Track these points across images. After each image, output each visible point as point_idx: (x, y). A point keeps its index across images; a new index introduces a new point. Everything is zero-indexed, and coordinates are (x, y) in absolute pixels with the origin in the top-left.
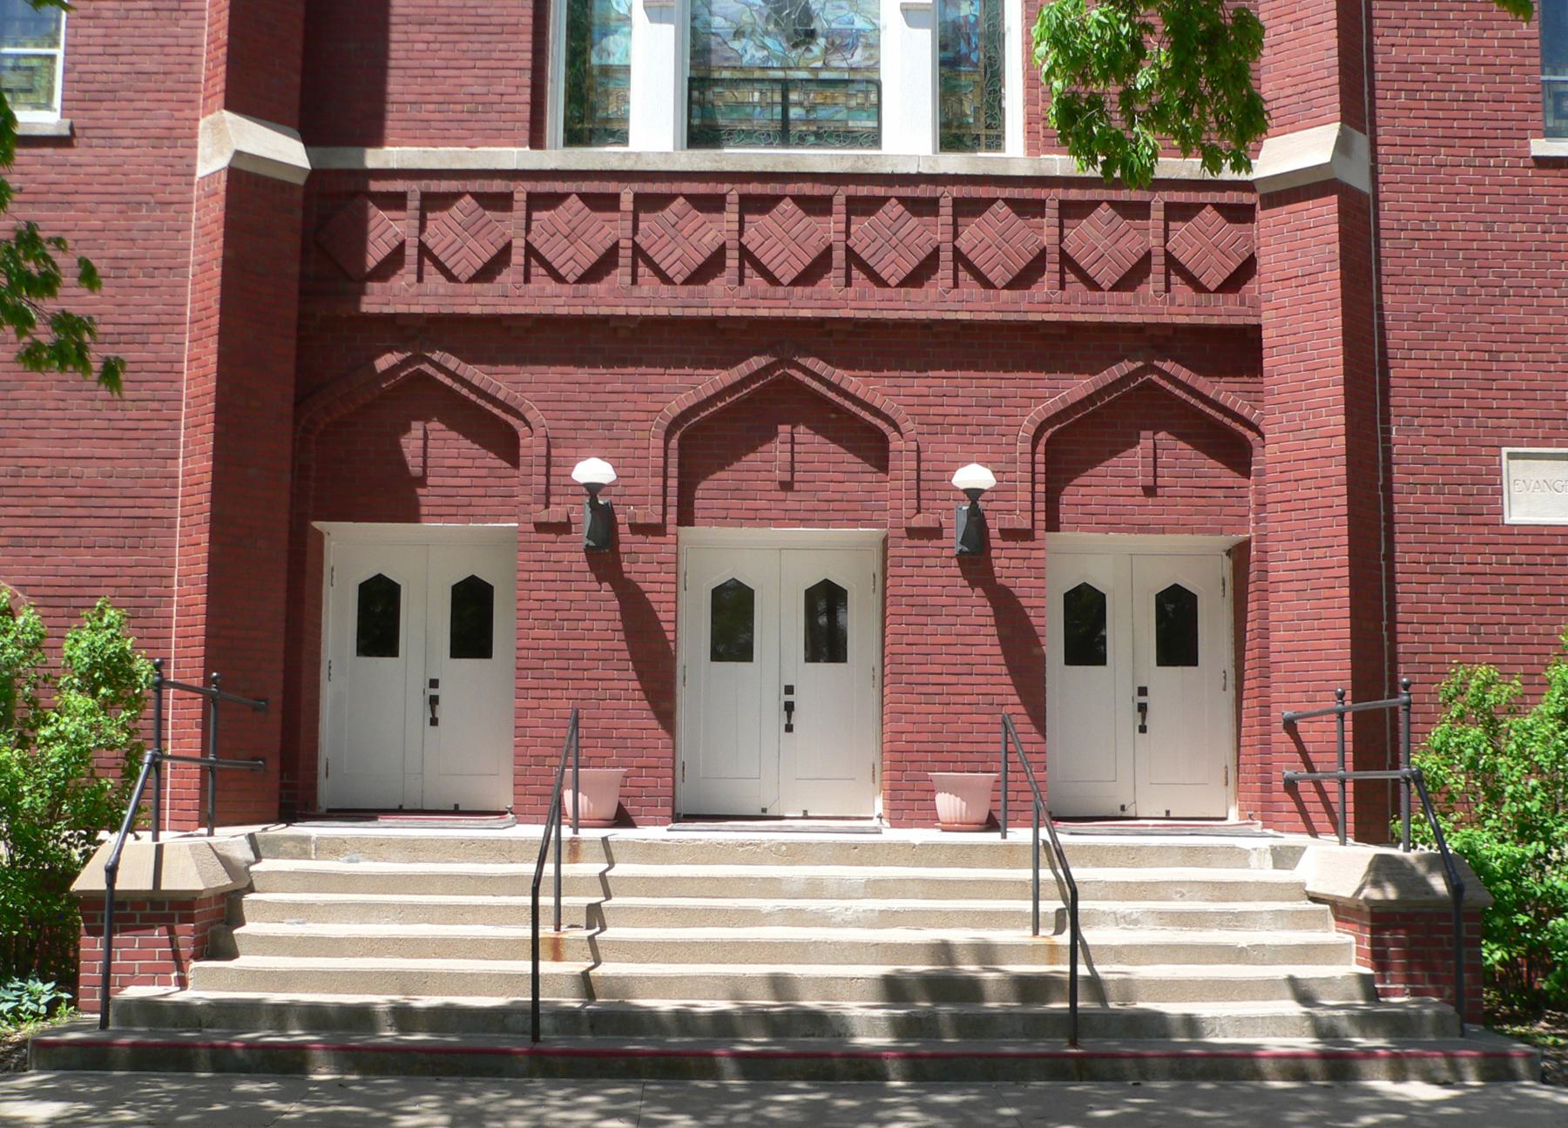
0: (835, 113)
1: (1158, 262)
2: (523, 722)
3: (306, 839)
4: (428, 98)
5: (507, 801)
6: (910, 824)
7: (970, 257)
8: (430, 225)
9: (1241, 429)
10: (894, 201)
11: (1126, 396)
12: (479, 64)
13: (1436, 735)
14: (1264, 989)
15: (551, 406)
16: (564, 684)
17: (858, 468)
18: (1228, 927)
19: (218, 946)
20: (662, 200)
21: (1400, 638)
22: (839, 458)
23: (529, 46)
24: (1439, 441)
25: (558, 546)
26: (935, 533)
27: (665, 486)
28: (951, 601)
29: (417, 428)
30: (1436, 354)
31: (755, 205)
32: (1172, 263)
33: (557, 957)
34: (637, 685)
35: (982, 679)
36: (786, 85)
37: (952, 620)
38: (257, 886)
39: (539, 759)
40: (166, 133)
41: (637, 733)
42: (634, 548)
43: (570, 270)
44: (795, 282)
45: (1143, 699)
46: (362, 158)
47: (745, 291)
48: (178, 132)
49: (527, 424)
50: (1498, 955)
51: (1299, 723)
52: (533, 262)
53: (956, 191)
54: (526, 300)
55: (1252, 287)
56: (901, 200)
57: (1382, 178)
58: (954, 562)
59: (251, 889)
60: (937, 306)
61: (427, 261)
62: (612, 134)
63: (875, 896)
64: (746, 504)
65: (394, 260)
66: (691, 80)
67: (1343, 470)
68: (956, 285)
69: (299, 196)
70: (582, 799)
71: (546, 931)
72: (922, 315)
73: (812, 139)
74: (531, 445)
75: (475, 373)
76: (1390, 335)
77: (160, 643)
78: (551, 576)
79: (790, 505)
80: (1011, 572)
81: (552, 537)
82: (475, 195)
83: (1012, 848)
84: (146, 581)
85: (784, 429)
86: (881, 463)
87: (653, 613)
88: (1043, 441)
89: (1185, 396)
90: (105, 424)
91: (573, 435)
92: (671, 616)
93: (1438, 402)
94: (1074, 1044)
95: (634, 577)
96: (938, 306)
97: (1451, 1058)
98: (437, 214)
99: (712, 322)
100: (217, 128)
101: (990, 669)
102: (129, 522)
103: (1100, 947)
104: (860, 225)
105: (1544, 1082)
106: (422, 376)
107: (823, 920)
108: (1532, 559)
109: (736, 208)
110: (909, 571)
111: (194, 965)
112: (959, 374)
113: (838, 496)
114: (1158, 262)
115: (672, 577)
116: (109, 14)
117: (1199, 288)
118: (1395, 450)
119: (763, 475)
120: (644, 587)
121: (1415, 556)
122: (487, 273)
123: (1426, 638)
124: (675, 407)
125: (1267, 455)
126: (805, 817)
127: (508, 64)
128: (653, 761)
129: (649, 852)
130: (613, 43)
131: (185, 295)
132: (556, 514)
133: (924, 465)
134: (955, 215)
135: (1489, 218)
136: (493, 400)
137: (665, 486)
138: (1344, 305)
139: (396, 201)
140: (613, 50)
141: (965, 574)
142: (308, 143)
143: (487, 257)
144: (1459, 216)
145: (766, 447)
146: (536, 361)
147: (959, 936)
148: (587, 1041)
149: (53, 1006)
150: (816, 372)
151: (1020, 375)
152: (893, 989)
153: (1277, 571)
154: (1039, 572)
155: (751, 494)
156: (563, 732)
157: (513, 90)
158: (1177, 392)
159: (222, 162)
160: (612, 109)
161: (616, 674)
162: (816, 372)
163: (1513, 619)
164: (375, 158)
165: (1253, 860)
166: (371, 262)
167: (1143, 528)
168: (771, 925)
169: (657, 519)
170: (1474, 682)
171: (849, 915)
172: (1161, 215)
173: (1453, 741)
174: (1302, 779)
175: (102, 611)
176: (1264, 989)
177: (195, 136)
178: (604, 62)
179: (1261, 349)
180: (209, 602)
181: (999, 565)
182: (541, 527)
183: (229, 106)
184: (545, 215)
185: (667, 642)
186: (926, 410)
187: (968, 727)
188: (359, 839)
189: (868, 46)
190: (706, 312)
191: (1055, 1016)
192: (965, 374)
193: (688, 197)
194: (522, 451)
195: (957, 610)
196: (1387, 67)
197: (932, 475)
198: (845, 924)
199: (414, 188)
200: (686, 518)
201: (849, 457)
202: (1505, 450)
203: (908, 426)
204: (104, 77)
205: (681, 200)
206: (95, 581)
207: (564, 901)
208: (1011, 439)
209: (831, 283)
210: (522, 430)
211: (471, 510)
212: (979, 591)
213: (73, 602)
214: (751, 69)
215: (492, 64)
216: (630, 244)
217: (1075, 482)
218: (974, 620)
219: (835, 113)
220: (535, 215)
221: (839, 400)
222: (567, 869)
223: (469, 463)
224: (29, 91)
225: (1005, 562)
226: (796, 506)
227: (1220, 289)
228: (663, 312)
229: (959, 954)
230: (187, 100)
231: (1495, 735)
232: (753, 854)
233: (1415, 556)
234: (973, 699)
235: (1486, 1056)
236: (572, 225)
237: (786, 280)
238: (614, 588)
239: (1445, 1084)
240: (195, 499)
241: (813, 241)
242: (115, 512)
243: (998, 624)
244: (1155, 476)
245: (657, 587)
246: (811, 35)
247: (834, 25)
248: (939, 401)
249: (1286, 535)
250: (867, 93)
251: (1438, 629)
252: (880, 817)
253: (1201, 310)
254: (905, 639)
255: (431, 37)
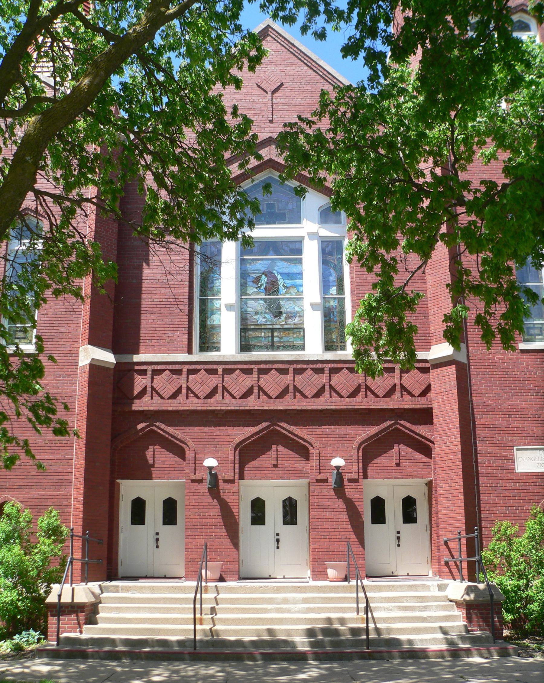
0: (290, 339)
1: (398, 387)
2: (187, 547)
3: (118, 586)
4: (154, 338)
5: (183, 574)
6: (319, 579)
7: (335, 387)
8: (155, 380)
9: (428, 443)
10: (309, 369)
11: (389, 433)
12: (170, 326)
13: (491, 546)
14: (432, 630)
15: (196, 440)
16: (201, 534)
17: (300, 459)
18: (421, 611)
19: (92, 620)
20: (232, 371)
21: (482, 512)
22: (293, 456)
23: (187, 320)
24: (493, 445)
25: (199, 487)
26: (325, 481)
27: (234, 467)
28: (332, 503)
29: (151, 448)
30: (491, 416)
31: (263, 372)
32: (403, 388)
33: (201, 624)
34: (226, 534)
35: (342, 530)
36: (273, 330)
37: (332, 510)
38: (102, 602)
39: (193, 559)
40: (69, 352)
41: (226, 550)
42: (224, 488)
43: (202, 395)
44: (276, 398)
45: (398, 535)
46: (132, 359)
47: (260, 401)
48: (72, 352)
49: (188, 446)
50: (510, 617)
51: (448, 542)
52: (189, 392)
53: (330, 365)
54: (187, 405)
55: (431, 395)
56: (312, 369)
57: (471, 358)
58: (332, 490)
59: (100, 603)
60: (324, 404)
61: (154, 392)
62: (215, 348)
63: (305, 603)
64: (262, 472)
65: (143, 392)
66: (241, 329)
67: (460, 457)
68: (331, 397)
69: (112, 372)
70: (208, 573)
71: (198, 616)
72: (319, 408)
73: (282, 348)
74: (189, 454)
75: (170, 430)
76: (475, 410)
77: (67, 521)
78: (196, 497)
79: (277, 472)
80: (351, 493)
81: (197, 484)
82: (170, 370)
83: (351, 586)
84: (63, 500)
85: (274, 447)
86: (307, 457)
87: (231, 509)
88: (361, 449)
89: (408, 432)
90: (49, 448)
91: (203, 449)
92: (237, 510)
93: (492, 432)
94: (368, 649)
95: (225, 497)
96: (324, 404)
97: (488, 649)
98: (157, 377)
99: (250, 411)
100: (86, 350)
101: (345, 526)
102: (56, 481)
103: (379, 618)
104: (298, 378)
105: (519, 656)
106: (153, 431)
107: (288, 611)
108: (525, 484)
109: (257, 373)
110: (317, 494)
111: (85, 626)
112: (332, 427)
113: (293, 469)
114: (398, 387)
115: (237, 497)
116: (51, 313)
117: (412, 396)
118: (478, 449)
119: (268, 462)
120: (228, 501)
121: (486, 485)
122: (174, 396)
123: (491, 512)
124: (237, 440)
125: (436, 451)
126: (284, 578)
127: (179, 326)
128: (232, 560)
129: (231, 590)
130: (214, 317)
131: (75, 405)
132: (198, 476)
133: (321, 458)
134: (330, 374)
135: (506, 370)
136: (176, 438)
137: (234, 467)
138: (459, 401)
139: (143, 373)
140: (214, 320)
141: (336, 495)
142: (114, 353)
143: (174, 391)
144: (497, 370)
145: (268, 453)
146: (190, 425)
147: (334, 615)
148: (211, 650)
149: (39, 640)
150: (285, 427)
151: (352, 426)
152: (310, 633)
153: (440, 491)
154: (361, 493)
155: (263, 469)
156: (201, 550)
157: (182, 335)
158: (406, 431)
159: (88, 362)
160: (215, 339)
161: (219, 530)
162: (285, 427)
163: (520, 505)
164: (137, 358)
165: (432, 589)
166: (136, 393)
167: (396, 477)
168: (271, 613)
169: (232, 478)
170: (503, 527)
171: (296, 609)
172: (399, 371)
173: (496, 547)
174: (450, 561)
175: (51, 512)
176: (432, 630)
177: (78, 353)
178: (212, 324)
179: (433, 416)
180: (84, 507)
181: (347, 491)
182: (193, 481)
183: (90, 343)
184: (193, 376)
185: (236, 519)
186: (321, 439)
187: (338, 546)
188: (135, 586)
189: (300, 316)
190: (247, 408)
191: (362, 640)
192: (334, 427)
193: (241, 370)
194: (186, 456)
195: (334, 507)
196: (471, 321)
197: (324, 461)
198: (295, 612)
199: (150, 368)
200: (242, 477)
201: (296, 455)
202: (515, 448)
203: (316, 445)
204: (49, 334)
205: (238, 370)
206: (46, 501)
207: (203, 606)
208: (350, 448)
209: (289, 397)
210: (186, 448)
211: (169, 475)
212: (341, 500)
213: (39, 507)
214: (261, 325)
215: (175, 326)
216: (221, 386)
217: (373, 462)
218: (339, 510)
219: (290, 339)
220: (190, 376)
221: (292, 436)
222: (204, 596)
223: (168, 459)
224: (25, 338)
225: (349, 490)
226: (278, 472)
227: (419, 396)
228: (233, 408)
229: (335, 622)
230: (75, 340)
231: (511, 545)
232: (265, 590)
233: (486, 485)
234: (340, 537)
235: (501, 649)
236: (202, 379)
237: (274, 397)
238: (218, 501)
239: (487, 658)
240: (79, 473)
241: (282, 383)
242: (52, 477)
243: (348, 511)
244: (400, 460)
245: (232, 501)
246: (281, 313)
247: (288, 310)
248: (326, 436)
249: (443, 479)
250: (300, 332)
251: (495, 509)
252: (309, 577)
253: (413, 403)
254: (316, 517)
255: (154, 318)
